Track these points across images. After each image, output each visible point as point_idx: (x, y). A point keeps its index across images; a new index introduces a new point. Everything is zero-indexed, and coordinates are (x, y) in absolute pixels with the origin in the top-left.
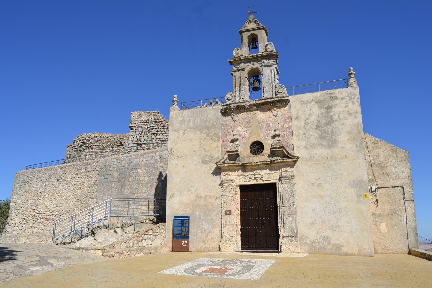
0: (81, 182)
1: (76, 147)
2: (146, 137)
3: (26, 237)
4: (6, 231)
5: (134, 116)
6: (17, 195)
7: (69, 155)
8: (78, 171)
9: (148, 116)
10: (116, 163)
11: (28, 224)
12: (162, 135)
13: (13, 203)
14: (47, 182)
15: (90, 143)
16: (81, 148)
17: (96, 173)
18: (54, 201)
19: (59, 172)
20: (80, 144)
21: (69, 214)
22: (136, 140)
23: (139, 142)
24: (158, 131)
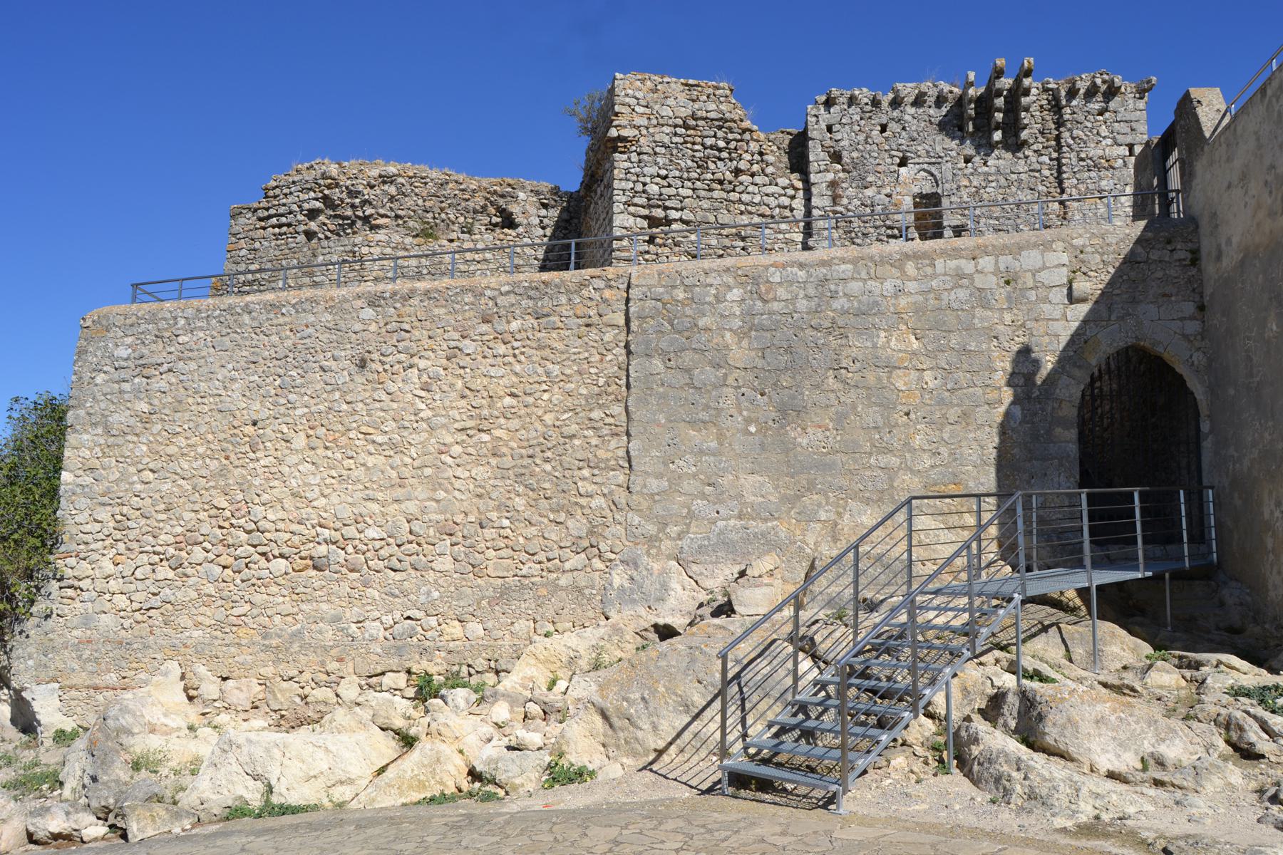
0: (514, 379)
1: (284, 220)
2: (690, 192)
3: (189, 651)
4: (48, 617)
5: (630, 92)
6: (100, 430)
7: (243, 252)
8: (486, 321)
9: (693, 101)
10: (736, 294)
11: (191, 581)
12: (756, 189)
13: (81, 473)
14: (293, 373)
15: (365, 202)
16: (312, 223)
17: (608, 337)
18: (345, 473)
19: (363, 322)
20: (306, 206)
21: (454, 539)
22: (643, 201)
23: (659, 210)
24: (737, 172)
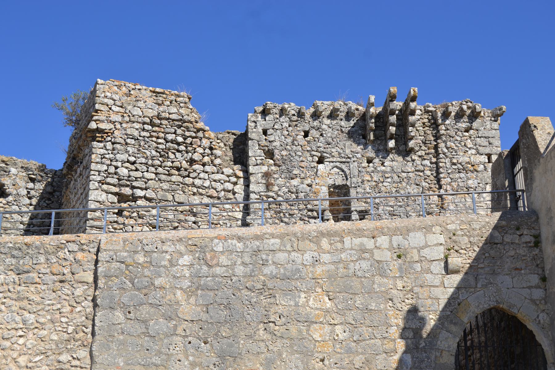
2: (153, 176)
5: (109, 94)
9: (159, 105)
10: (186, 259)
12: (206, 176)
17: (78, 292)
22: (114, 181)
23: (128, 189)
24: (192, 162)
